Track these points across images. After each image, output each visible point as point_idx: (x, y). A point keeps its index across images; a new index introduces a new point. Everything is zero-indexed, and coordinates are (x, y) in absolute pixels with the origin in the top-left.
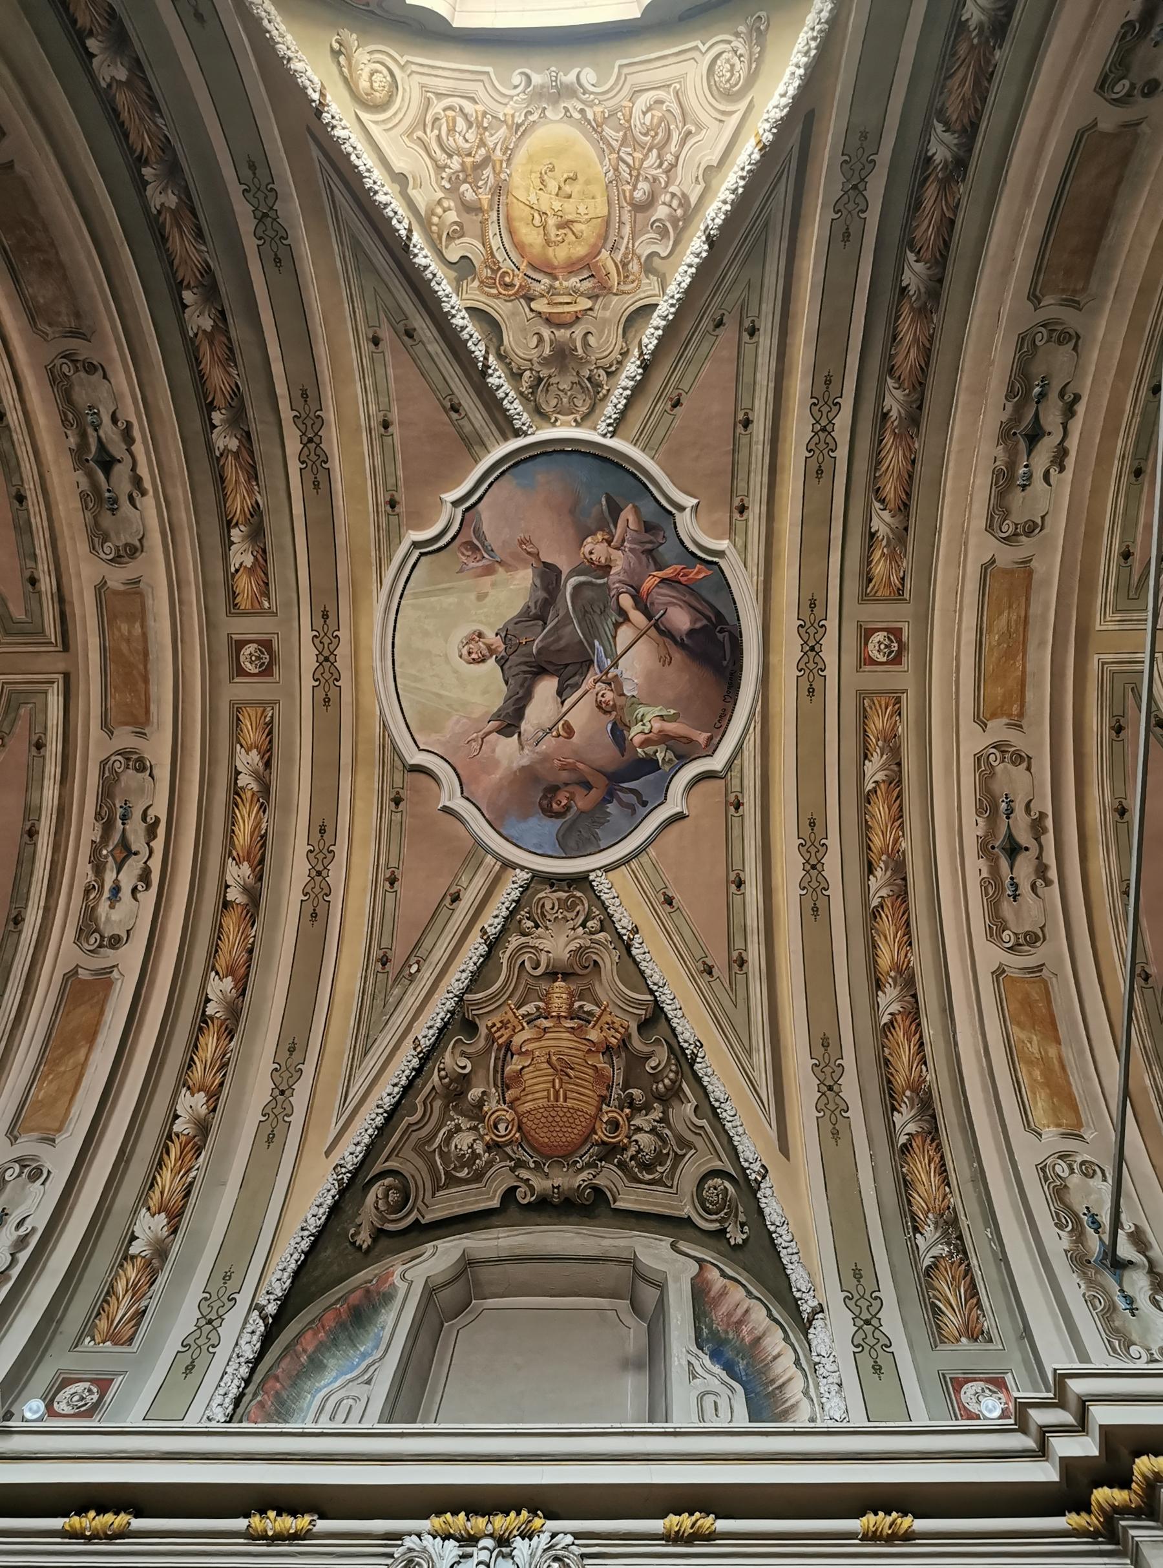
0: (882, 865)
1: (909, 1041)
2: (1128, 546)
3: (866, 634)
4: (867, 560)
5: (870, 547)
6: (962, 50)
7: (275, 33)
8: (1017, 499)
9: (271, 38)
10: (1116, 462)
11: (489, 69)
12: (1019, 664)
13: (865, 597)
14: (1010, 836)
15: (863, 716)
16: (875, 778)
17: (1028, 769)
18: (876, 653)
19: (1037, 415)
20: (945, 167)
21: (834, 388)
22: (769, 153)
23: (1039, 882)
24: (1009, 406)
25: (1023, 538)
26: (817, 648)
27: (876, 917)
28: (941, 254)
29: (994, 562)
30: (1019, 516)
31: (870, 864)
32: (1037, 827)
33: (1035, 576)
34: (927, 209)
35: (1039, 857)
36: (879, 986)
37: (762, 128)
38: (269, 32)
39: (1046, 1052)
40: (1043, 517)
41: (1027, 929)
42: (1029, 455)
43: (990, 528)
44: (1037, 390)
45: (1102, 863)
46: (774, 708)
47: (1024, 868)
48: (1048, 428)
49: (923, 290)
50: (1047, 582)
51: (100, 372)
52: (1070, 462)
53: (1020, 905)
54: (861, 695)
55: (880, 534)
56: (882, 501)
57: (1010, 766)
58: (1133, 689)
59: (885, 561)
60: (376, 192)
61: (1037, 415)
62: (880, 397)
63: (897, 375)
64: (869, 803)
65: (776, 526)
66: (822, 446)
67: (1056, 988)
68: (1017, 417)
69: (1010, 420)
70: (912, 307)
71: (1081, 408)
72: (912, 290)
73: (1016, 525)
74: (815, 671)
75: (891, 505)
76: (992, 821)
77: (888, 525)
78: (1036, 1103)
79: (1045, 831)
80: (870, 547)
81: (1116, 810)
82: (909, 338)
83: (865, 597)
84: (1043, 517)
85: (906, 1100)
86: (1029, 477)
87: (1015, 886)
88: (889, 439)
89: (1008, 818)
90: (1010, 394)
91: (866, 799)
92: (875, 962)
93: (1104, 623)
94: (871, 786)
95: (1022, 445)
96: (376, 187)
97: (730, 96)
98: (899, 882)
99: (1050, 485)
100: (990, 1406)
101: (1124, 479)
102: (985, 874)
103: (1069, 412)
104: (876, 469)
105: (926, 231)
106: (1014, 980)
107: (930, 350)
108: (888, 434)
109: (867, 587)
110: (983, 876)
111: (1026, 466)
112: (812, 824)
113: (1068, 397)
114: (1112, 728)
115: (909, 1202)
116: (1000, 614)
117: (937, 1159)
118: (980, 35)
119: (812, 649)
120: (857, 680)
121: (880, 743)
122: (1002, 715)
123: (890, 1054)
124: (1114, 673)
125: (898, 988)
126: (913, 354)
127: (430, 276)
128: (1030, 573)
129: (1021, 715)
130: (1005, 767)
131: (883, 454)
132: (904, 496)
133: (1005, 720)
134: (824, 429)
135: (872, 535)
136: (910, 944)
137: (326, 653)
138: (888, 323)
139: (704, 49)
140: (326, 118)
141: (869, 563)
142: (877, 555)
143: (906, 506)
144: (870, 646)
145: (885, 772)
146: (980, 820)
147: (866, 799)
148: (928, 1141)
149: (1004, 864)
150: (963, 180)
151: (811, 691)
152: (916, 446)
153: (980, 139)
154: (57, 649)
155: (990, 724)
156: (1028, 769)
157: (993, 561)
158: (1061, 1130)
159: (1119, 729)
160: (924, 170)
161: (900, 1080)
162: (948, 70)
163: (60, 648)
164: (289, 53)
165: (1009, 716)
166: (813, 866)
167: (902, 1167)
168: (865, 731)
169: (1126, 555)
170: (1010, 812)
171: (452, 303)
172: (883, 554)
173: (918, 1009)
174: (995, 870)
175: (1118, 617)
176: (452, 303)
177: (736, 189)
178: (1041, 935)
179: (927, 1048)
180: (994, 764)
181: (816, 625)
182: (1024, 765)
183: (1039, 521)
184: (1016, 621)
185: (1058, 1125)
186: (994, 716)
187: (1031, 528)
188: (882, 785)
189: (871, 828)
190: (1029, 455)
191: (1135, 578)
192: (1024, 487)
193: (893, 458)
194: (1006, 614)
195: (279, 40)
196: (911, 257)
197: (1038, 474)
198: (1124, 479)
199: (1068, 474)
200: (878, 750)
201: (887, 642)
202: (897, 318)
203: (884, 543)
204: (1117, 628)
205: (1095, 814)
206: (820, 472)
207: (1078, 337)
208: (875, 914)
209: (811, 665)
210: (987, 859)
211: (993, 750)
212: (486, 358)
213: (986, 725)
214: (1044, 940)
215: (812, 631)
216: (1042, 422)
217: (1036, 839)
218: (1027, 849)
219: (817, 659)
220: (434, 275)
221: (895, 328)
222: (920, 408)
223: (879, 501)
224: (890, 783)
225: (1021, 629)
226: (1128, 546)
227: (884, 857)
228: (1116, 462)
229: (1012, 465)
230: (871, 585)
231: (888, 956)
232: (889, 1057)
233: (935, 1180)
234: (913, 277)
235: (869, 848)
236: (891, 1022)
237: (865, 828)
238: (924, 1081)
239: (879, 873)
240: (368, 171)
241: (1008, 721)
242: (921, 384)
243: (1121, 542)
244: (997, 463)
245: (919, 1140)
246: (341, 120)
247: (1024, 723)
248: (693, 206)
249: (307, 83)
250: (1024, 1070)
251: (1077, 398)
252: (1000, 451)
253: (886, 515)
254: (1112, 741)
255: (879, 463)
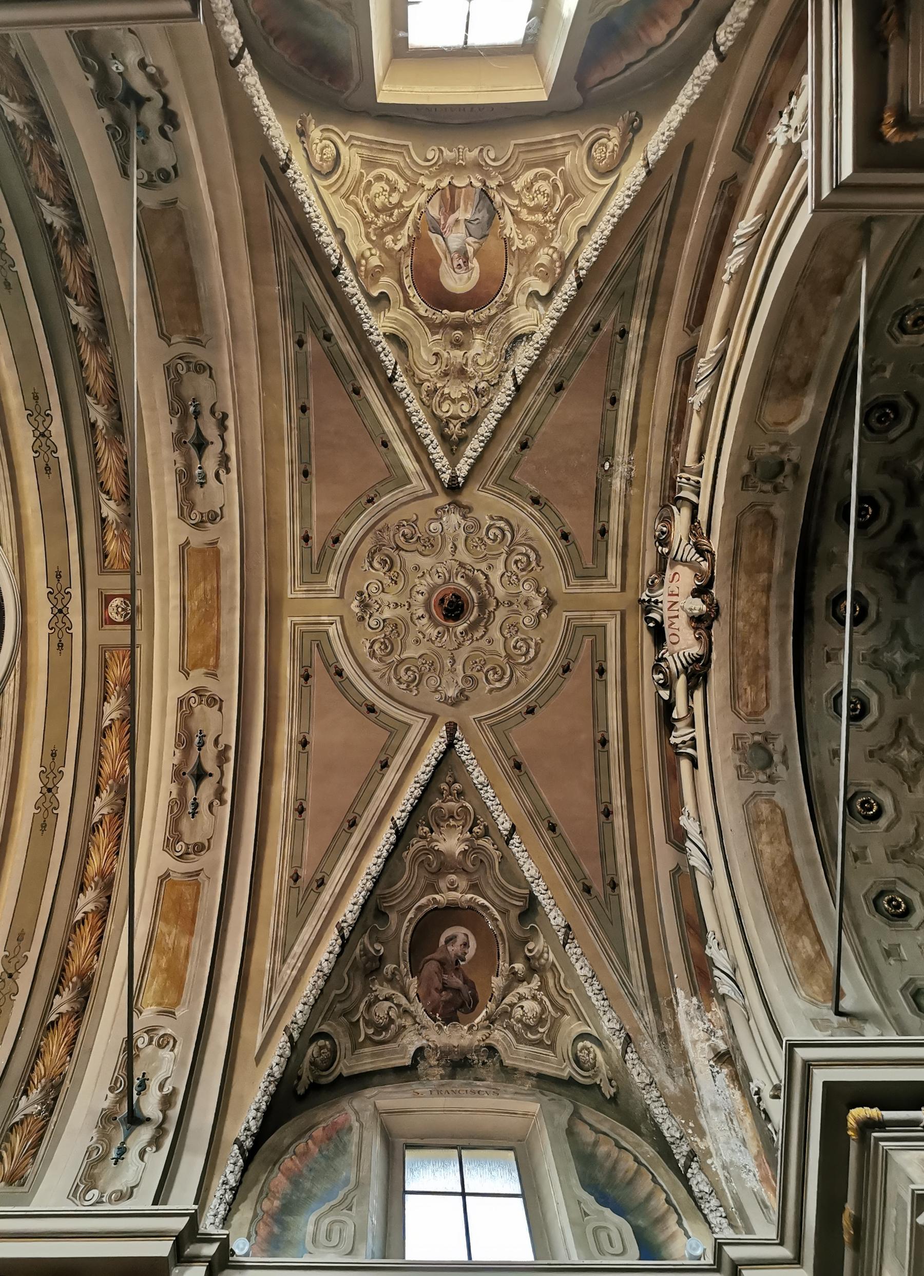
0: (108, 788)
1: (92, 935)
2: (307, 532)
3: (107, 600)
4: (102, 540)
5: (103, 529)
6: (26, 144)
7: (261, 108)
8: (198, 493)
9: (259, 112)
10: (287, 466)
11: (410, 144)
12: (215, 625)
13: (103, 570)
14: (199, 765)
15: (105, 666)
16: (112, 717)
17: (220, 710)
18: (115, 615)
19: (198, 428)
20: (66, 232)
21: (42, 401)
22: (624, 219)
23: (216, 802)
24: (175, 420)
25: (209, 525)
26: (64, 610)
27: (94, 831)
28: (94, 299)
29: (189, 543)
30: (202, 507)
31: (98, 787)
32: (222, 757)
33: (222, 555)
34: (68, 267)
35: (220, 782)
36: (82, 889)
37: (621, 200)
38: (258, 107)
39: (179, 943)
40: (221, 509)
41: (198, 840)
42: (200, 459)
43: (181, 516)
44: (192, 409)
45: (283, 786)
46: (31, 659)
47: (207, 789)
48: (210, 439)
49: (91, 328)
50: (231, 559)
51: (208, 371)
52: (233, 464)
53: (196, 821)
54: (103, 649)
55: (110, 519)
56: (107, 493)
57: (206, 708)
58: (318, 645)
59: (117, 540)
60: (320, 234)
61: (198, 428)
62: (85, 411)
63: (94, 393)
64: (105, 737)
65: (22, 511)
66: (44, 448)
67: (205, 891)
68: (183, 429)
69: (178, 432)
70: (87, 340)
71: (230, 423)
72: (82, 327)
73: (202, 514)
74: (63, 630)
75: (116, 496)
76: (186, 753)
77: (114, 511)
78: (151, 985)
79: (227, 760)
80: (103, 529)
81: (300, 742)
82: (93, 365)
83: (103, 570)
84: (221, 509)
85: (71, 985)
86: (204, 477)
87: (196, 805)
88: (101, 444)
89: (199, 749)
90: (172, 412)
91: (103, 733)
92: (85, 868)
93: (293, 592)
94: (107, 723)
95: (194, 452)
96: (322, 231)
97: (604, 174)
98: (119, 801)
99: (221, 483)
100: (694, 1246)
101: (296, 479)
102: (174, 796)
103: (222, 425)
104: (96, 468)
105: (74, 280)
106: (175, 883)
107: (114, 374)
108: (99, 438)
109: (104, 562)
110: (173, 796)
111: (200, 468)
112: (54, 755)
113: (219, 415)
114: (301, 676)
115: (33, 1069)
116: (198, 584)
117: (72, 1034)
118: (31, 131)
119: (60, 612)
120: (97, 637)
121: (117, 688)
122: (201, 667)
123: (73, 947)
124: (303, 632)
125: (98, 891)
126: (101, 377)
127: (356, 302)
128: (218, 553)
129: (216, 666)
130: (202, 708)
131: (99, 455)
132: (124, 489)
133: (204, 670)
134: (43, 435)
135: (103, 520)
136: (118, 854)
137: (60, 606)
138: (72, 352)
139: (583, 138)
140: (290, 173)
141: (104, 542)
142: (110, 536)
143: (127, 497)
144: (110, 609)
145: (120, 712)
146: (177, 751)
147: (103, 733)
148: (73, 1019)
149: (191, 787)
150: (86, 242)
151: (60, 646)
152: (125, 449)
153: (82, 211)
154: (615, 590)
155: (191, 673)
156: (220, 710)
157: (187, 543)
158: (161, 1008)
159: (307, 677)
160: (51, 235)
161: (73, 968)
162: (24, 159)
163: (618, 589)
164: (270, 123)
165: (207, 667)
166: (49, 790)
167: (42, 1040)
168: (106, 678)
169: (306, 539)
170: (201, 745)
171: (371, 323)
172: (114, 535)
173: (108, 908)
174: (182, 793)
175: (305, 587)
176: (371, 323)
177: (623, 206)
178: (207, 845)
179: (105, 941)
180: (193, 706)
181: (62, 592)
182: (217, 707)
183: (219, 512)
184: (210, 590)
185: (159, 1004)
186: (195, 667)
187: (214, 517)
188: (117, 723)
189: (103, 757)
190: (200, 459)
191: (315, 557)
192: (202, 484)
193: (109, 459)
194: (202, 585)
195: (265, 113)
196: (71, 301)
197: (211, 475)
198: (296, 479)
199: (234, 474)
200: (116, 694)
201: (124, 606)
202: (79, 349)
203: (114, 526)
204: (304, 596)
205: (283, 746)
206: (48, 469)
207: (211, 369)
208: (94, 829)
209: (60, 625)
210: (179, 783)
211: (194, 695)
212: (395, 368)
213: (188, 674)
214: (209, 848)
215: (59, 597)
216: (204, 433)
217: (219, 767)
218: (211, 775)
219: (65, 620)
220: (359, 302)
221: (80, 357)
222: (120, 419)
223: (104, 493)
224: (123, 721)
225: (215, 596)
226: (307, 532)
227: (110, 782)
228: (287, 466)
229: (189, 467)
230: (107, 560)
231: (96, 864)
232: (72, 950)
233: (63, 1050)
234: (79, 318)
235: (100, 774)
236: (83, 919)
237: (99, 757)
238: (92, 968)
239: (104, 795)
240: (317, 217)
241: (205, 670)
242: (115, 401)
243: (301, 528)
244: (178, 465)
245: (65, 1019)
246: (301, 175)
247: (219, 672)
248: (566, 257)
249: (280, 146)
250: (154, 957)
251: (225, 416)
252: (176, 456)
253: (112, 504)
254: (301, 686)
255: (98, 462)
